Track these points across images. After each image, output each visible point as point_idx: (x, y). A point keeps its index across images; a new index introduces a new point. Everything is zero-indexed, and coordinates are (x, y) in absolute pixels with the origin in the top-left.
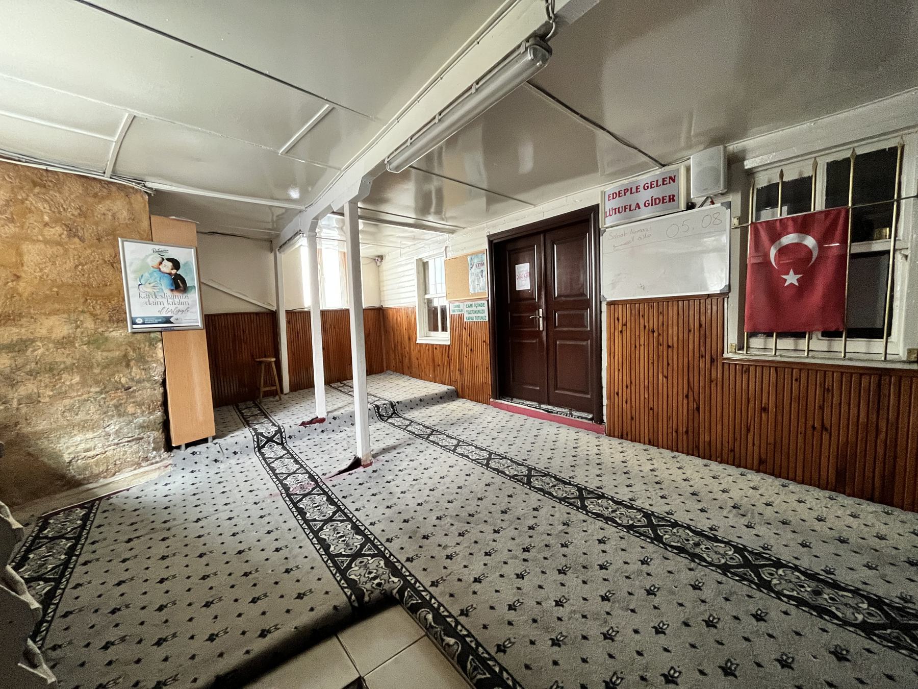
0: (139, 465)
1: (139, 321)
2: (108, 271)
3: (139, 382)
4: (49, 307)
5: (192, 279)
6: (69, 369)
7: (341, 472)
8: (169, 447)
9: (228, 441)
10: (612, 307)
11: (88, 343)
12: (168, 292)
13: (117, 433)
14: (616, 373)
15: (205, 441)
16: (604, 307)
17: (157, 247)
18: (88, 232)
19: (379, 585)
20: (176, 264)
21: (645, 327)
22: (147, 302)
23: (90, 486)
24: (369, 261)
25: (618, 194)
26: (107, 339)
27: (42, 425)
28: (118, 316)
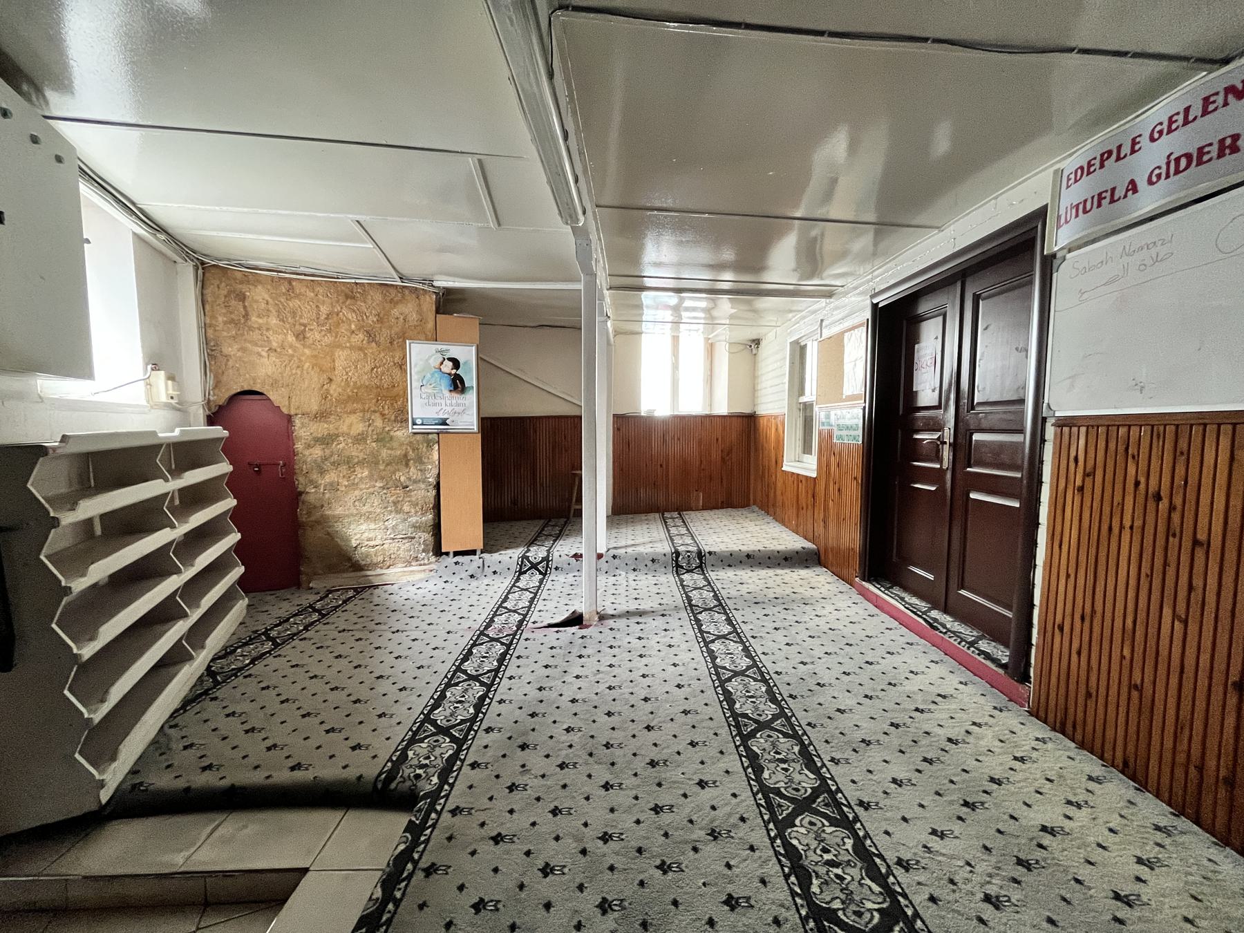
0: (409, 563)
1: (419, 421)
2: (397, 371)
3: (415, 482)
4: (349, 407)
5: (471, 380)
6: (361, 463)
7: (550, 626)
8: (438, 552)
9: (492, 558)
10: (1066, 429)
11: (377, 441)
12: (447, 394)
13: (394, 528)
14: (1062, 581)
15: (473, 552)
16: (1050, 432)
17: (439, 347)
18: (383, 337)
19: (418, 777)
20: (456, 363)
21: (1137, 484)
22: (429, 402)
23: (369, 573)
24: (742, 347)
25: (1086, 170)
26: (391, 438)
27: (339, 511)
28: (401, 416)
